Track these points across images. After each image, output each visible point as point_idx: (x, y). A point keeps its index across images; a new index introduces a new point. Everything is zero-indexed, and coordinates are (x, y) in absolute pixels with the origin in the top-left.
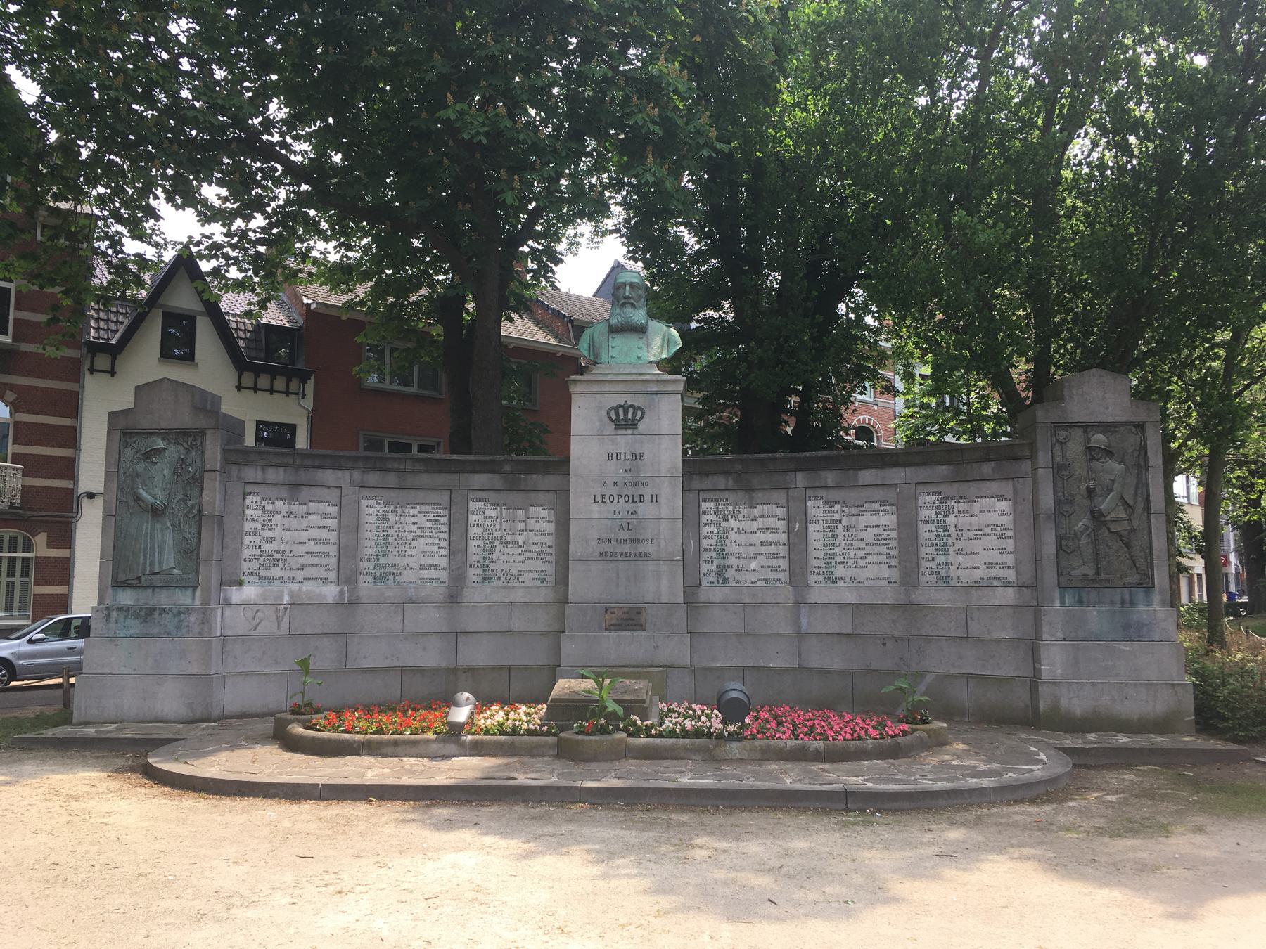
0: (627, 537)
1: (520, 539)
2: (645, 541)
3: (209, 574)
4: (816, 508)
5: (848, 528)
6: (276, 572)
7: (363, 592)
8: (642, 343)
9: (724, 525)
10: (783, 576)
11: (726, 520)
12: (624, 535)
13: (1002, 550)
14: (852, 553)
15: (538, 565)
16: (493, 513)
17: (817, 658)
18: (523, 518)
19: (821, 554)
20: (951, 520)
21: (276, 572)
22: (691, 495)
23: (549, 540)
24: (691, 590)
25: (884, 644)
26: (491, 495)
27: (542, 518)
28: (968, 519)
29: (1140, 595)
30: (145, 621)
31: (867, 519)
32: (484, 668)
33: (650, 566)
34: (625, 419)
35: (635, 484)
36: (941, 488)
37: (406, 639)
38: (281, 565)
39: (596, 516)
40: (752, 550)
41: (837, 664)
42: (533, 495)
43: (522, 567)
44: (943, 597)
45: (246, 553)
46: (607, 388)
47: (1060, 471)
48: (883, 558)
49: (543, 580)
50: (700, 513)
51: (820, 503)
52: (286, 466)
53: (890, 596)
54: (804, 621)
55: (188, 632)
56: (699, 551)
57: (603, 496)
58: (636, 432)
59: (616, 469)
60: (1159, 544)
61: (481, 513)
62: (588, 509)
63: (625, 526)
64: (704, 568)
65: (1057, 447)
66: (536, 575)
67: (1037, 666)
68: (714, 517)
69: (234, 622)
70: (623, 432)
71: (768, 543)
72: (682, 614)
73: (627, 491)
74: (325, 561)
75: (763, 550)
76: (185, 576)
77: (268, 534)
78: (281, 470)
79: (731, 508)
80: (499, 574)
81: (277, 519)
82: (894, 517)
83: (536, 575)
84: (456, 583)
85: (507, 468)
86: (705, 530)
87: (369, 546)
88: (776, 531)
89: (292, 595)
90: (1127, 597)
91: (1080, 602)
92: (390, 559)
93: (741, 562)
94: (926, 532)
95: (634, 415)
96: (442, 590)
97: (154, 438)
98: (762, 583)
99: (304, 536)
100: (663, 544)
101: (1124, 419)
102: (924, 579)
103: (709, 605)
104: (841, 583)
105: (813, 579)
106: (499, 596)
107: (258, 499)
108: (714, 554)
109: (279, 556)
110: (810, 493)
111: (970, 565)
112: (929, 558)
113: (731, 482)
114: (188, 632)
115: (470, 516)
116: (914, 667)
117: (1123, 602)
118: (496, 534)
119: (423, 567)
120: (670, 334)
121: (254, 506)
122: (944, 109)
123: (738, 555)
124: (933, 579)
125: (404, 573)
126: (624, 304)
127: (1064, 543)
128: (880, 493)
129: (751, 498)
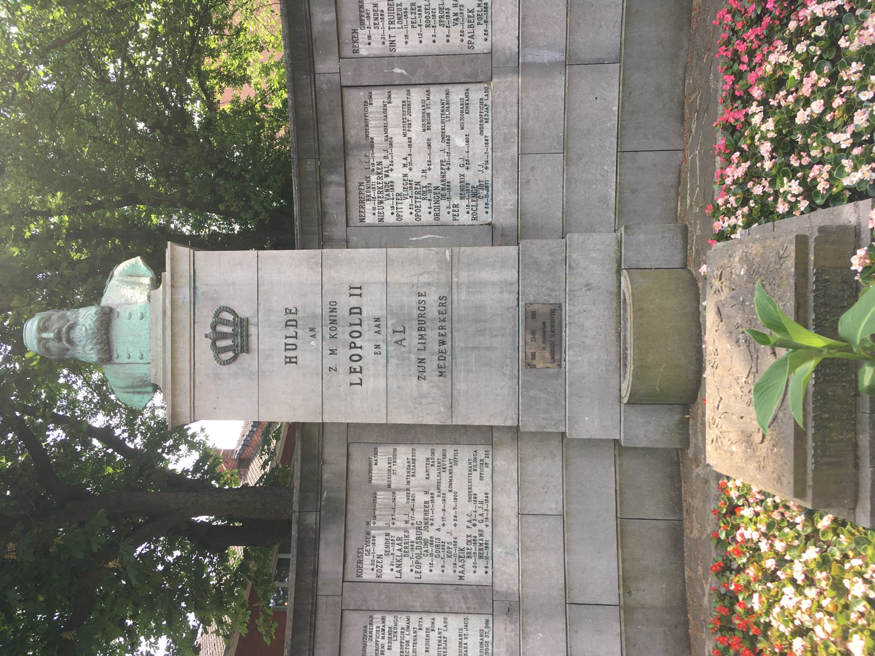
0: (416, 334)
1: (421, 499)
2: (422, 307)
4: (371, 42)
8: (124, 314)
9: (399, 188)
10: (477, 93)
11: (391, 186)
12: (412, 338)
16: (380, 541)
18: (389, 494)
19: (441, 32)
22: (354, 239)
23: (422, 454)
24: (494, 234)
26: (353, 544)
27: (389, 465)
33: (461, 298)
34: (234, 337)
35: (333, 322)
39: (382, 382)
40: (437, 145)
42: (353, 478)
43: (463, 495)
46: (184, 365)
49: (483, 464)
50: (381, 225)
51: (362, 34)
54: (547, 56)
57: (352, 371)
58: (253, 321)
59: (310, 352)
61: (381, 560)
62: (378, 392)
63: (398, 337)
64: (464, 218)
66: (476, 475)
68: (387, 204)
70: (253, 340)
72: (534, 247)
73: (344, 333)
75: (436, 126)
79: (374, 178)
80: (474, 532)
83: (476, 475)
84: (486, 601)
85: (311, 519)
86: (408, 217)
88: (407, 106)
93: (455, 161)
95: (226, 323)
98: (488, 127)
100: (425, 278)
103: (520, 211)
105: (481, 45)
106: (508, 531)
108: (444, 203)
110: (347, 51)
113: (336, 178)
118: (413, 537)
120: (121, 274)
122: (286, 157)
123: (445, 165)
126: (70, 341)
129: (359, 146)
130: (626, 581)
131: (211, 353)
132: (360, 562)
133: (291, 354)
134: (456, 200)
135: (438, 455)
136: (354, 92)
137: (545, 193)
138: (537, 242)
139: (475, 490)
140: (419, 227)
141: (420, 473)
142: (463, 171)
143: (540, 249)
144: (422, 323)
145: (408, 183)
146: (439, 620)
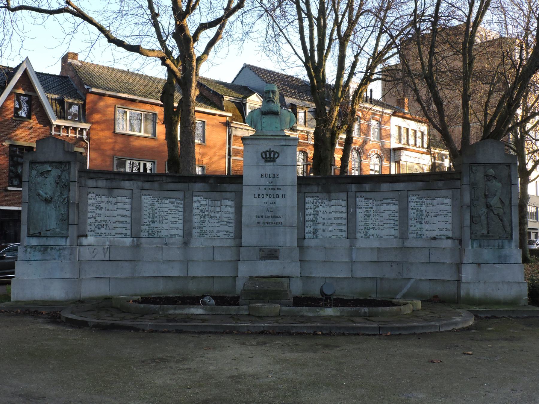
0: (270, 215)
1: (218, 215)
2: (278, 217)
3: (73, 231)
4: (361, 202)
5: (376, 211)
6: (103, 230)
7: (143, 241)
10: (345, 234)
12: (269, 214)
13: (446, 222)
14: (377, 223)
15: (226, 228)
16: (205, 203)
17: (360, 273)
19: (362, 223)
20: (424, 208)
21: (103, 230)
23: (232, 216)
24: (301, 239)
25: (392, 266)
28: (432, 208)
29: (506, 242)
30: (43, 253)
31: (385, 207)
32: (202, 277)
35: (274, 189)
36: (420, 193)
37: (164, 263)
38: (105, 227)
39: (255, 204)
40: (330, 221)
41: (370, 275)
42: (224, 194)
43: (219, 229)
44: (419, 244)
45: (89, 221)
47: (472, 185)
48: (392, 226)
50: (305, 203)
51: (362, 199)
52: (107, 179)
53: (395, 243)
55: (64, 259)
56: (304, 222)
57: (259, 195)
59: (265, 182)
60: (515, 220)
62: (249, 199)
64: (307, 230)
65: (472, 175)
66: (225, 233)
67: (460, 275)
68: (312, 205)
69: (86, 254)
70: (269, 164)
71: (338, 218)
72: (297, 251)
73: (271, 192)
74: (125, 225)
75: (335, 221)
76: (62, 232)
77: (98, 212)
78: (105, 181)
79: (320, 201)
80: (208, 232)
81: (103, 205)
82: (397, 206)
83: (225, 233)
86: (307, 212)
87: (146, 219)
88: (341, 212)
89: (110, 242)
90: (501, 244)
91: (480, 247)
92: (156, 225)
93: (325, 227)
94: (412, 213)
95: (274, 155)
96: (181, 240)
97: (45, 166)
98: (334, 237)
99: (115, 213)
101: (502, 162)
102: (411, 236)
104: (372, 237)
105: (358, 235)
107: (94, 195)
108: (312, 223)
109: (104, 223)
110: (358, 194)
111: (432, 229)
112: (413, 227)
113: (320, 188)
114: (64, 259)
115: (194, 204)
116: (405, 276)
117: (498, 246)
118: (206, 213)
119: (171, 229)
121: (92, 199)
123: (323, 224)
124: (415, 235)
125: (162, 231)
126: (268, 101)
127: (474, 219)
128: (391, 195)
129: (330, 197)
130: (194, 278)
131: (265, 150)
132: (198, 196)
133: (264, 175)
134: (312, 227)
135: (231, 221)
136: (346, 196)
137: (313, 255)
138: (298, 252)
139: (221, 232)
140: (304, 215)
141: (226, 215)
142: (322, 230)
143: (296, 253)
144: (274, 217)
145: (318, 212)
146: (181, 221)
